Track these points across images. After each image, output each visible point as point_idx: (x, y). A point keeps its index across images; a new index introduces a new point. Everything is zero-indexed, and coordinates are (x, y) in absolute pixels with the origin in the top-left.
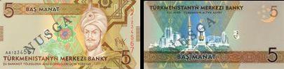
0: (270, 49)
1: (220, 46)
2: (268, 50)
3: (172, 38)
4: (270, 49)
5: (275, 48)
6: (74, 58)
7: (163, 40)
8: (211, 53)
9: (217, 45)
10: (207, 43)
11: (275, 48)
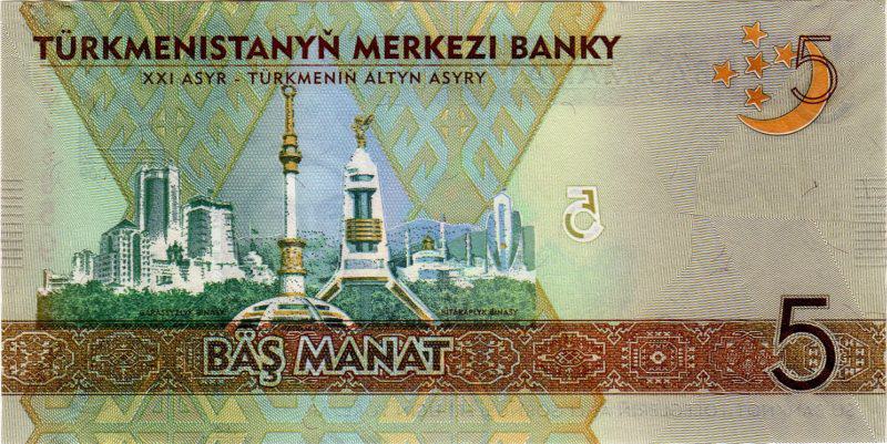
0: (789, 304)
1: (479, 283)
2: (774, 313)
3: (178, 234)
4: (789, 304)
5: (820, 302)
6: (431, 46)
7: (123, 247)
8: (417, 327)
9: (467, 275)
10: (397, 263)
11: (820, 302)
